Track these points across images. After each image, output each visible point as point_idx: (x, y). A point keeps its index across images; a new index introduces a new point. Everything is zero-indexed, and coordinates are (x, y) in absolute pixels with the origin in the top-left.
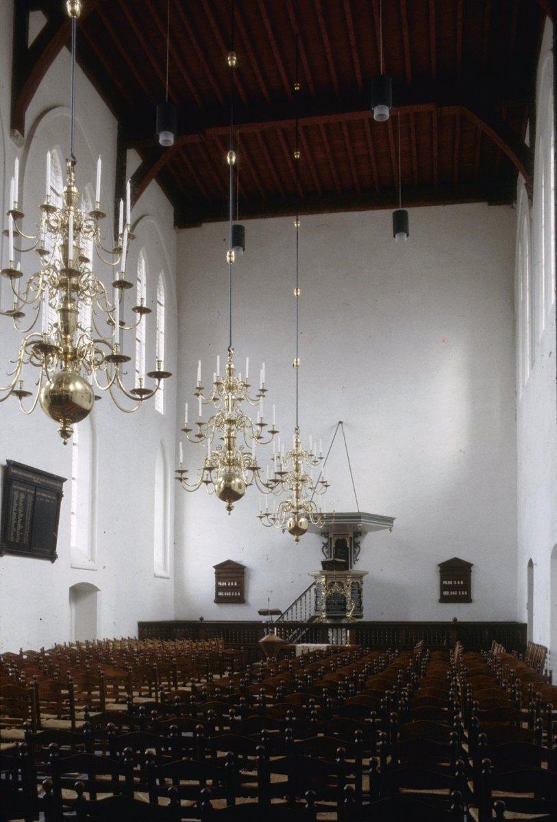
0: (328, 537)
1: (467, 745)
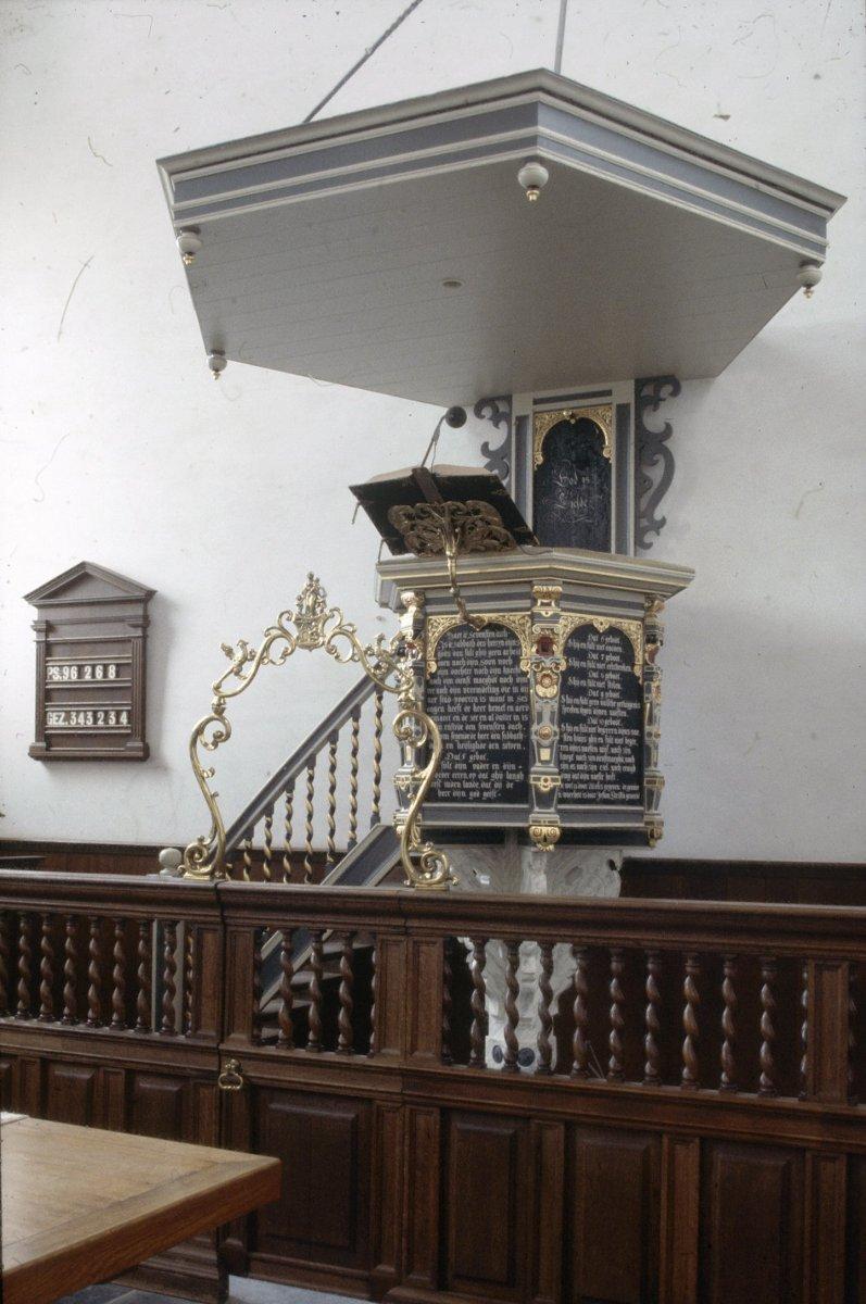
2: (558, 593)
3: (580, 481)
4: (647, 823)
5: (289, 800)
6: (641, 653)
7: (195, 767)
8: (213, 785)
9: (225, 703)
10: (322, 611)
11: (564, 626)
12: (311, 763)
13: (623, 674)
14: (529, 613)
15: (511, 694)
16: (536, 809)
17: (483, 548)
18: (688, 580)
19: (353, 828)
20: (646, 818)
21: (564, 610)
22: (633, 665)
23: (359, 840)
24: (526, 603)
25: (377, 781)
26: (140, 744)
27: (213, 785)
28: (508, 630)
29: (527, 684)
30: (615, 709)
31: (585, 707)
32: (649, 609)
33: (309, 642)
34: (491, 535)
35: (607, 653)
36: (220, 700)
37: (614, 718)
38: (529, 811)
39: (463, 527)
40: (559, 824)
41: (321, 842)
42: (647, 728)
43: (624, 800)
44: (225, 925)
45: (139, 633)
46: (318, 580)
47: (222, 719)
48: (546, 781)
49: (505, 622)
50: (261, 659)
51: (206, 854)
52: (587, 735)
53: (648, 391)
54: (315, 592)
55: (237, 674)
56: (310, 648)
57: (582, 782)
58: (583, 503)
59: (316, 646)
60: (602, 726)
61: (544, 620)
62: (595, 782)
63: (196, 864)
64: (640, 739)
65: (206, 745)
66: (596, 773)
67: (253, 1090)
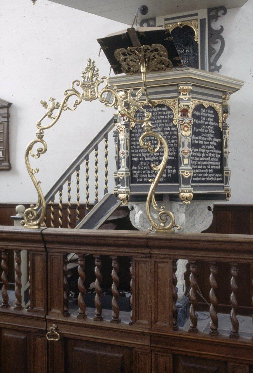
2: (190, 89)
3: (185, 52)
4: (226, 190)
5: (69, 184)
6: (221, 118)
7: (28, 168)
8: (38, 177)
9: (43, 133)
10: (96, 79)
11: (192, 105)
12: (78, 169)
13: (215, 126)
14: (177, 99)
15: (169, 135)
16: (182, 186)
17: (157, 69)
18: (241, 86)
19: (97, 195)
20: (225, 188)
21: (192, 98)
22: (218, 123)
23: (99, 200)
24: (175, 94)
25: (106, 175)
26: (8, 164)
27: (38, 177)
28: (167, 107)
29: (177, 130)
30: (212, 141)
31: (201, 140)
32: (224, 99)
33: (90, 97)
34: (162, 62)
35: (209, 117)
36: (40, 131)
37: (212, 145)
38: (179, 186)
39: (149, 58)
40: (193, 192)
41: (83, 201)
42: (225, 150)
43: (216, 181)
44: (47, 252)
45: (6, 120)
46: (94, 62)
47: (42, 142)
48: (187, 173)
49: (164, 103)
50: (63, 107)
51: (35, 213)
52: (202, 153)
53: (213, 13)
54: (93, 69)
55: (50, 116)
56: (90, 100)
57: (200, 173)
58: (186, 60)
59: (94, 99)
60: (207, 149)
61: (184, 101)
62: (205, 173)
63: (30, 220)
64: (222, 154)
65: (33, 156)
66: (205, 169)
67: (65, 339)
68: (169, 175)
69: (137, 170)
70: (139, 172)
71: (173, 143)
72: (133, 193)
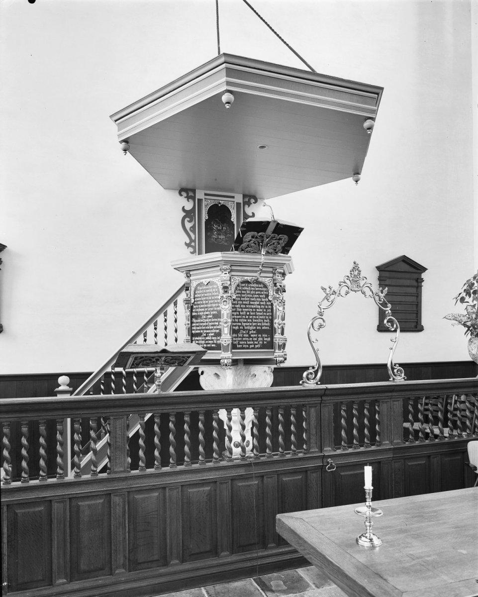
0: (193, 198)
1: (224, 428)
3: (222, 229)
28: (263, 284)
38: (274, 352)
68: (265, 342)
69: (237, 337)
70: (239, 339)
71: (268, 316)
72: (233, 358)
